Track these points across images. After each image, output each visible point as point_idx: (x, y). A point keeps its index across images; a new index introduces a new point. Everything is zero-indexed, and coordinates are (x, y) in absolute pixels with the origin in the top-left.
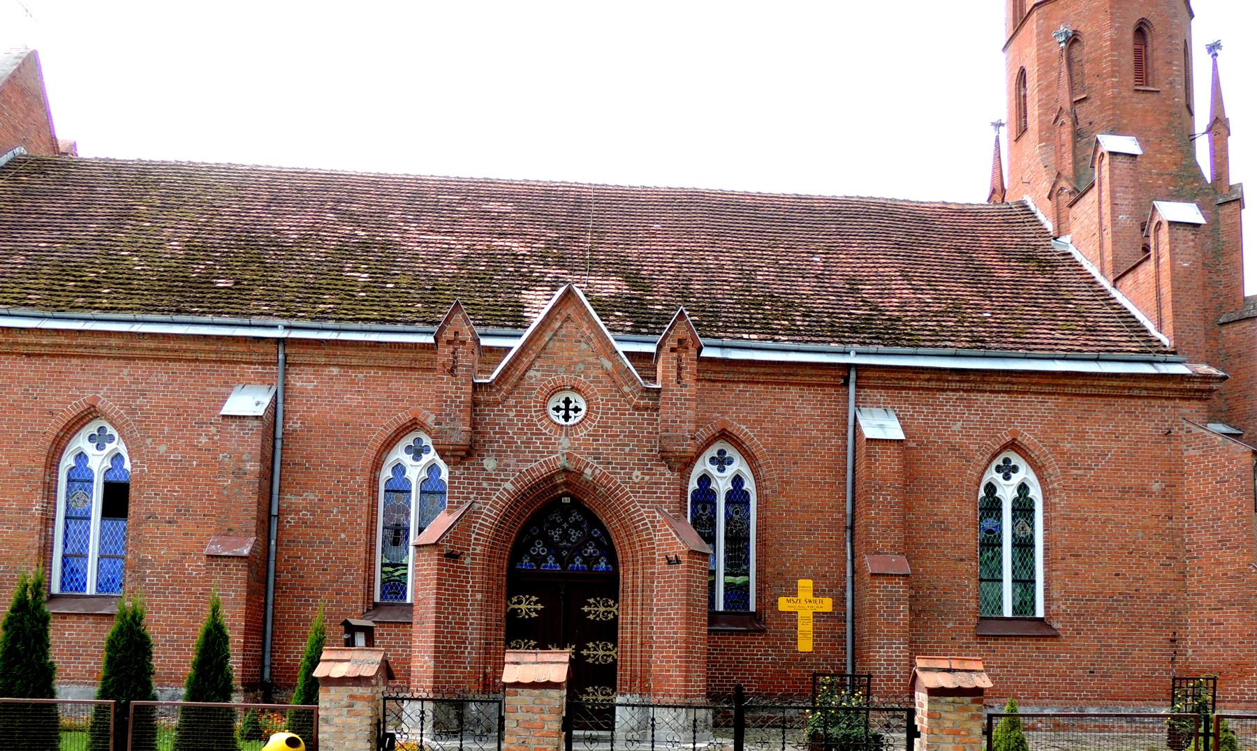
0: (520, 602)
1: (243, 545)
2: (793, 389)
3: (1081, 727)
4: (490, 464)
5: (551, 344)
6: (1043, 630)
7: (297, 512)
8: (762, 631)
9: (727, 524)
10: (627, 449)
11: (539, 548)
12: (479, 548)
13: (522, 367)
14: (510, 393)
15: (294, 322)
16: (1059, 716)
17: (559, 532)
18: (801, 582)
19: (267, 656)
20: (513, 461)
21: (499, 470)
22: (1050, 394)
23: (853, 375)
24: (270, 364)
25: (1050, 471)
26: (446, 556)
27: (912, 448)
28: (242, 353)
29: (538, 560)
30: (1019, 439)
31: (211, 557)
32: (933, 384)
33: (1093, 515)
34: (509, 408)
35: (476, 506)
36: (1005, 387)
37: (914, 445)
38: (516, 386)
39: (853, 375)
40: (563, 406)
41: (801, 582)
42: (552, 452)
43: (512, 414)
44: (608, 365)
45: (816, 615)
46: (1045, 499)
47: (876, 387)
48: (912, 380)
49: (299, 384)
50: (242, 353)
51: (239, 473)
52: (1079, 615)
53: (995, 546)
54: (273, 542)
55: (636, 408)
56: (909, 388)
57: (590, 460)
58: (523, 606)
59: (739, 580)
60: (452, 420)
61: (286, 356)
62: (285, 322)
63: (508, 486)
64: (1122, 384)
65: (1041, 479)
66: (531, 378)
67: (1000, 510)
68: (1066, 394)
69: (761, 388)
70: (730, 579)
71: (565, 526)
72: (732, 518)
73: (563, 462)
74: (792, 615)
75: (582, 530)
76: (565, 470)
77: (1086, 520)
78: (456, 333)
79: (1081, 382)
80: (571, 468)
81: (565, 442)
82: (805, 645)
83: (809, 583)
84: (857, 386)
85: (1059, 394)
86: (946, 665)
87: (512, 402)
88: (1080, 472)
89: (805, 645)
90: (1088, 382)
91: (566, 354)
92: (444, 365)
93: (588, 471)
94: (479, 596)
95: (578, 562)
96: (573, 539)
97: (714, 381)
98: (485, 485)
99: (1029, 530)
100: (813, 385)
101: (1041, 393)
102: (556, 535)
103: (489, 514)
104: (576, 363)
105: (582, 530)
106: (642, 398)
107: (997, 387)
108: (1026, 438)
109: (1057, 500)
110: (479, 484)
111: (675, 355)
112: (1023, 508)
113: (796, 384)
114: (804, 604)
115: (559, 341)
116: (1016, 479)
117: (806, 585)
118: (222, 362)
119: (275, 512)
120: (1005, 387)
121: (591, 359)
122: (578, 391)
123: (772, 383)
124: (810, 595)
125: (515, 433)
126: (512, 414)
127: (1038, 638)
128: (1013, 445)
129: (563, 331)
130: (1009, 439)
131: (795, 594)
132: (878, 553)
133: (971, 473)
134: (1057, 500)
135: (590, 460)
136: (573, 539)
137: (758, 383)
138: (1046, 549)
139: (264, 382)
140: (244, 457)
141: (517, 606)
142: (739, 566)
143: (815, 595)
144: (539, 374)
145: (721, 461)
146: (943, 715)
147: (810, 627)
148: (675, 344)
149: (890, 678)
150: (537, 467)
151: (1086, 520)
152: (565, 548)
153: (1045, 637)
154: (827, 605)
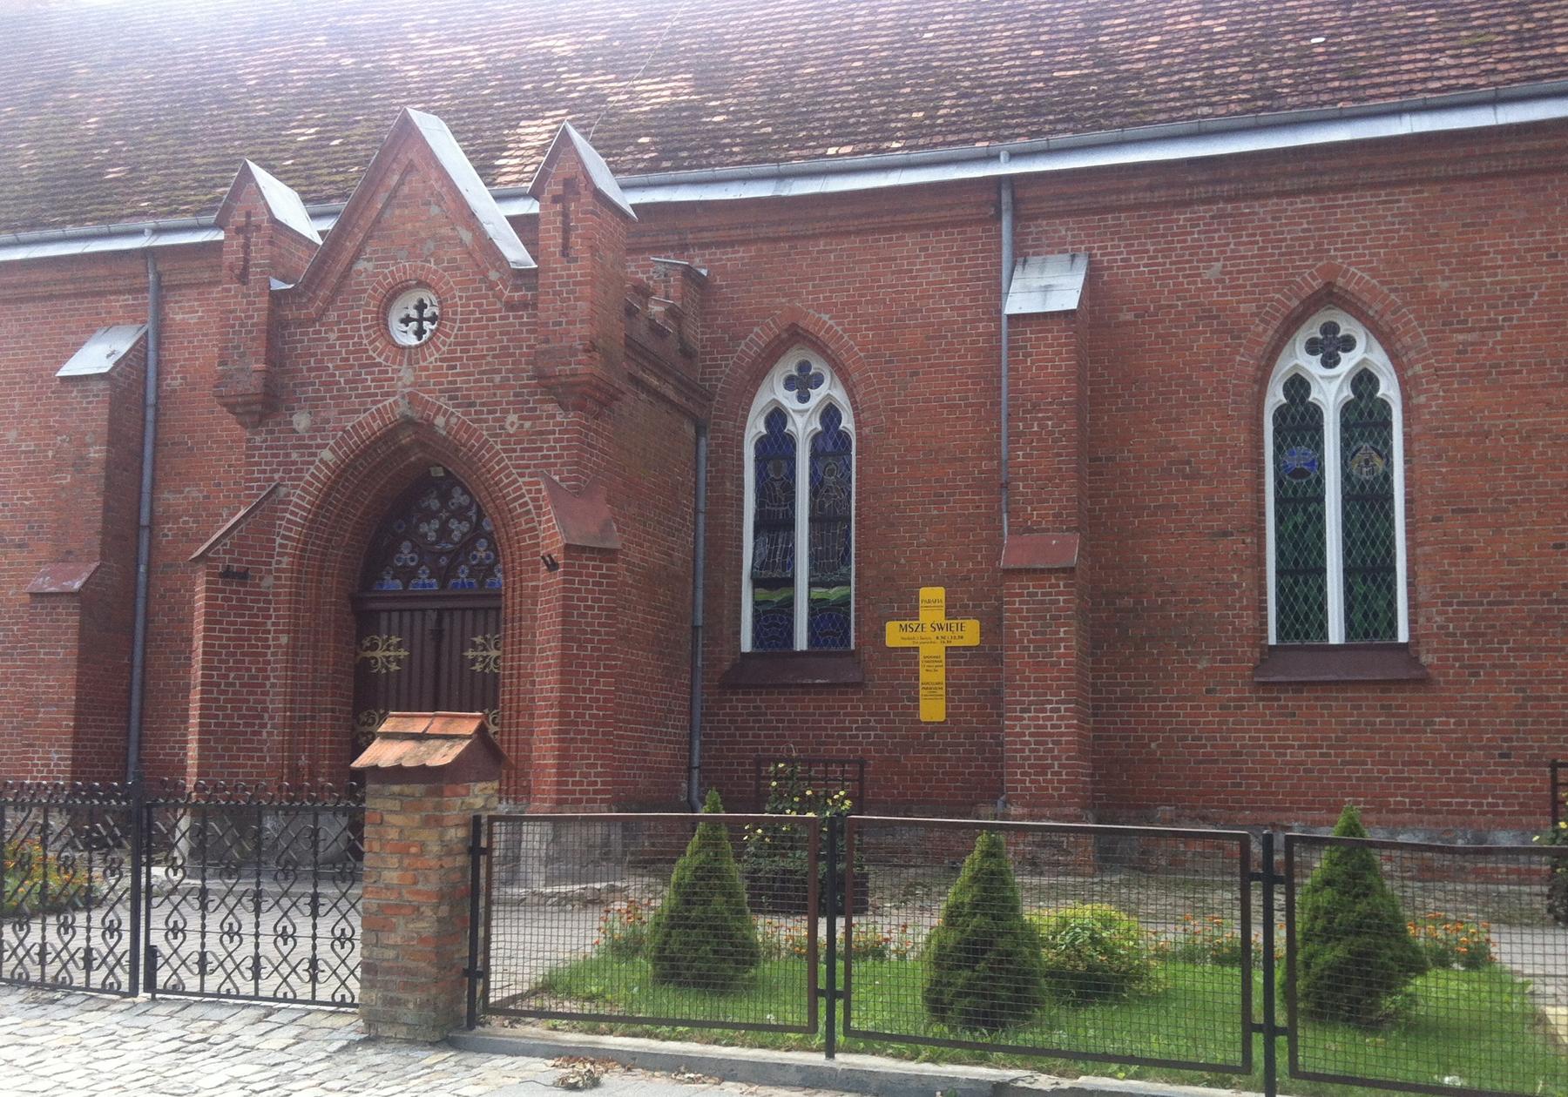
0: (374, 647)
1: (73, 576)
2: (910, 239)
3: (1478, 872)
4: (301, 421)
5: (387, 215)
6: (1406, 674)
7: (176, 521)
8: (858, 685)
9: (814, 493)
10: (497, 378)
11: (406, 554)
12: (285, 559)
13: (345, 257)
14: (330, 301)
15: (163, 222)
16: (1430, 848)
17: (454, 524)
18: (926, 593)
19: (133, 748)
20: (333, 413)
21: (315, 429)
22: (1401, 183)
23: (1006, 197)
24: (137, 291)
25: (1407, 340)
26: (222, 575)
27: (1127, 323)
28: (105, 278)
29: (408, 574)
30: (1340, 281)
31: (37, 596)
32: (1161, 195)
33: (1501, 424)
34: (329, 327)
35: (283, 490)
36: (1303, 182)
37: (1130, 316)
38: (337, 290)
39: (1006, 197)
40: (414, 314)
41: (926, 593)
42: (388, 394)
43: (333, 336)
44: (467, 236)
45: (952, 653)
46: (1406, 398)
47: (1058, 215)
48: (1119, 191)
49: (178, 317)
50: (105, 278)
51: (80, 464)
52: (1474, 636)
53: (1309, 501)
54: (142, 569)
55: (510, 306)
56: (1121, 209)
57: (443, 402)
58: (379, 654)
59: (834, 593)
60: (242, 355)
61: (159, 276)
62: (151, 223)
63: (326, 455)
64: (1551, 143)
65: (1394, 357)
66: (359, 273)
67: (1319, 429)
68: (1437, 180)
69: (856, 242)
70: (819, 592)
71: (444, 515)
72: (822, 483)
73: (403, 408)
74: (910, 654)
75: (468, 519)
76: (408, 422)
77: (1487, 435)
78: (248, 215)
79: (1461, 152)
80: (416, 416)
81: (407, 375)
82: (932, 709)
83: (939, 593)
84: (1016, 218)
85: (1421, 181)
86: (419, 726)
87: (333, 316)
88: (1470, 337)
89: (932, 709)
90: (1477, 150)
91: (409, 226)
92: (231, 268)
93: (440, 421)
94: (284, 639)
95: (463, 573)
96: (456, 536)
97: (776, 240)
98: (294, 456)
99: (1379, 464)
100: (943, 225)
101: (1385, 185)
102: (430, 530)
103: (299, 501)
104: (423, 241)
105: (468, 519)
106: (516, 288)
107: (1288, 185)
108: (1356, 278)
109: (1422, 399)
110: (287, 455)
111: (559, 207)
112: (1364, 416)
113: (916, 227)
114: (930, 632)
115: (401, 206)
116: (1348, 362)
117: (932, 596)
118: (83, 295)
119: (145, 521)
120: (1303, 182)
121: (446, 231)
122: (428, 286)
123: (873, 231)
124: (939, 616)
125: (337, 368)
126: (333, 336)
127: (1386, 685)
128: (1329, 296)
129: (406, 189)
130: (1317, 284)
131: (914, 615)
132: (1030, 530)
133: (1245, 360)
134: (1422, 399)
135: (443, 402)
136: (456, 536)
137: (849, 233)
138: (1409, 501)
139: (135, 321)
140: (88, 439)
141: (369, 654)
142: (834, 569)
143: (948, 615)
144: (370, 266)
145: (802, 383)
146: (387, 818)
147: (939, 676)
148: (558, 189)
149: (1043, 770)
150: (368, 420)
151: (1487, 435)
152: (442, 553)
153: (1400, 683)
154: (969, 633)
